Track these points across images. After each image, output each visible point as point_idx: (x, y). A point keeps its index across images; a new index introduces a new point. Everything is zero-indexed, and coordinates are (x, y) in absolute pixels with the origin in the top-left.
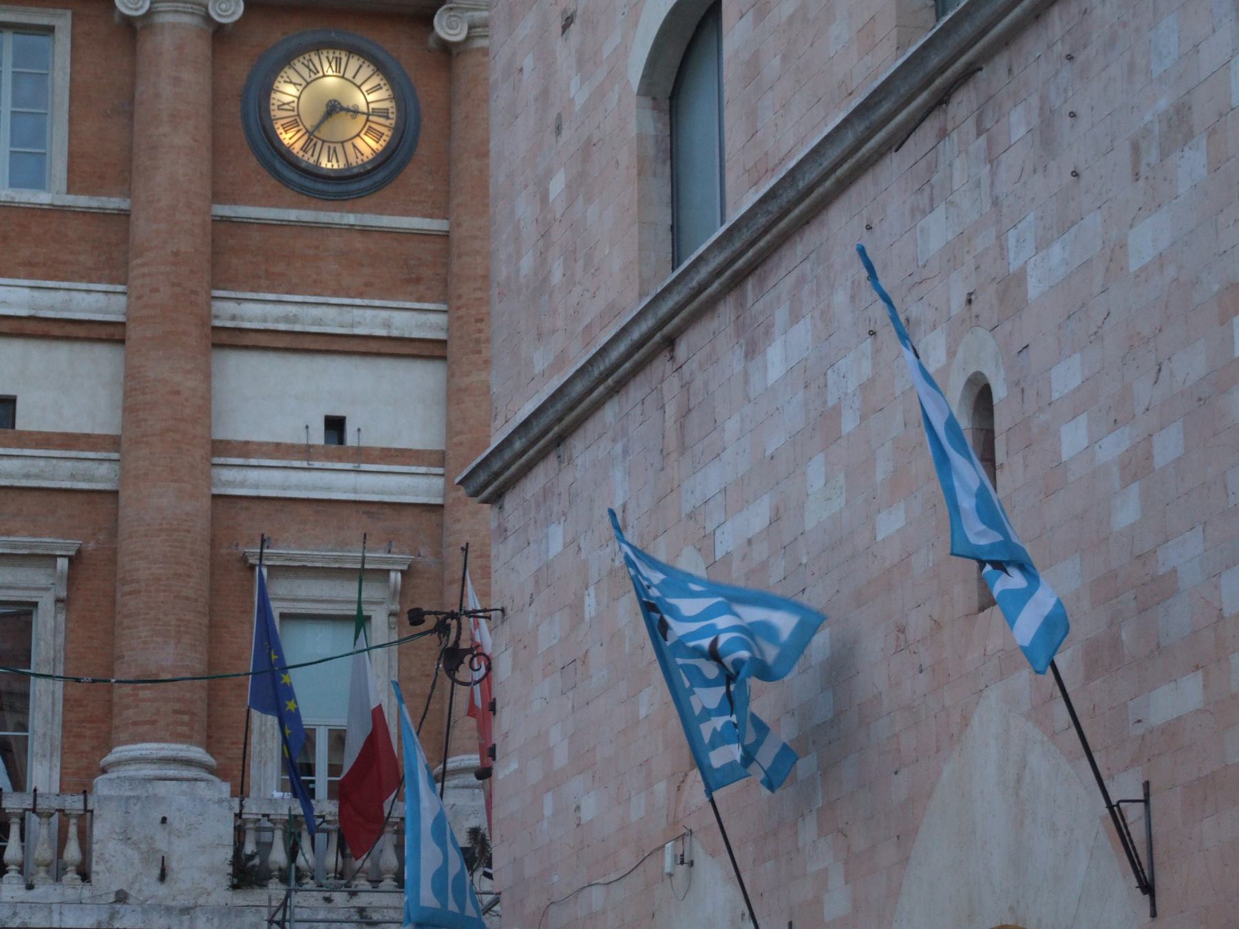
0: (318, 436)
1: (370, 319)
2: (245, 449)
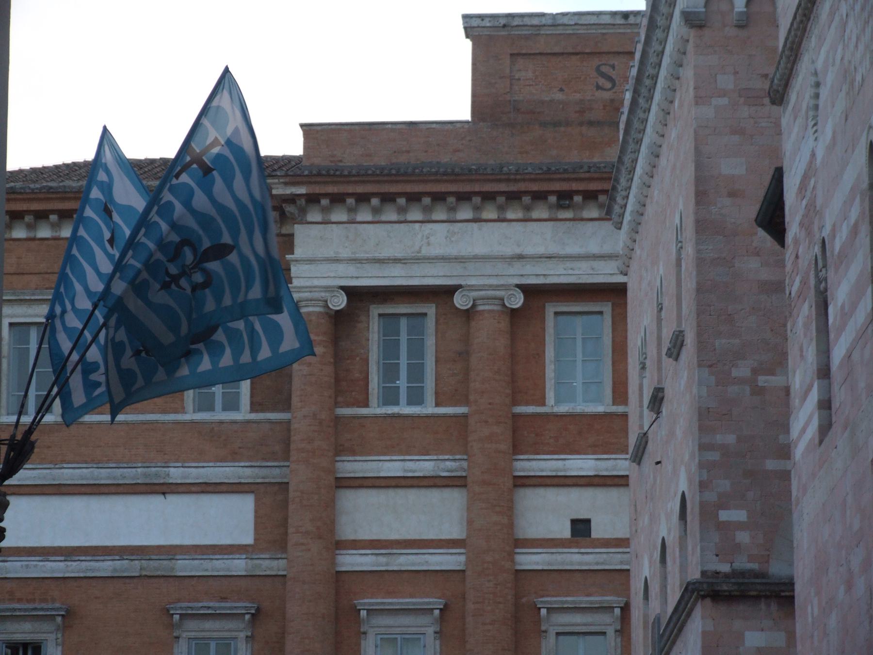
0: (567, 533)
1: (425, 466)
2: (356, 544)
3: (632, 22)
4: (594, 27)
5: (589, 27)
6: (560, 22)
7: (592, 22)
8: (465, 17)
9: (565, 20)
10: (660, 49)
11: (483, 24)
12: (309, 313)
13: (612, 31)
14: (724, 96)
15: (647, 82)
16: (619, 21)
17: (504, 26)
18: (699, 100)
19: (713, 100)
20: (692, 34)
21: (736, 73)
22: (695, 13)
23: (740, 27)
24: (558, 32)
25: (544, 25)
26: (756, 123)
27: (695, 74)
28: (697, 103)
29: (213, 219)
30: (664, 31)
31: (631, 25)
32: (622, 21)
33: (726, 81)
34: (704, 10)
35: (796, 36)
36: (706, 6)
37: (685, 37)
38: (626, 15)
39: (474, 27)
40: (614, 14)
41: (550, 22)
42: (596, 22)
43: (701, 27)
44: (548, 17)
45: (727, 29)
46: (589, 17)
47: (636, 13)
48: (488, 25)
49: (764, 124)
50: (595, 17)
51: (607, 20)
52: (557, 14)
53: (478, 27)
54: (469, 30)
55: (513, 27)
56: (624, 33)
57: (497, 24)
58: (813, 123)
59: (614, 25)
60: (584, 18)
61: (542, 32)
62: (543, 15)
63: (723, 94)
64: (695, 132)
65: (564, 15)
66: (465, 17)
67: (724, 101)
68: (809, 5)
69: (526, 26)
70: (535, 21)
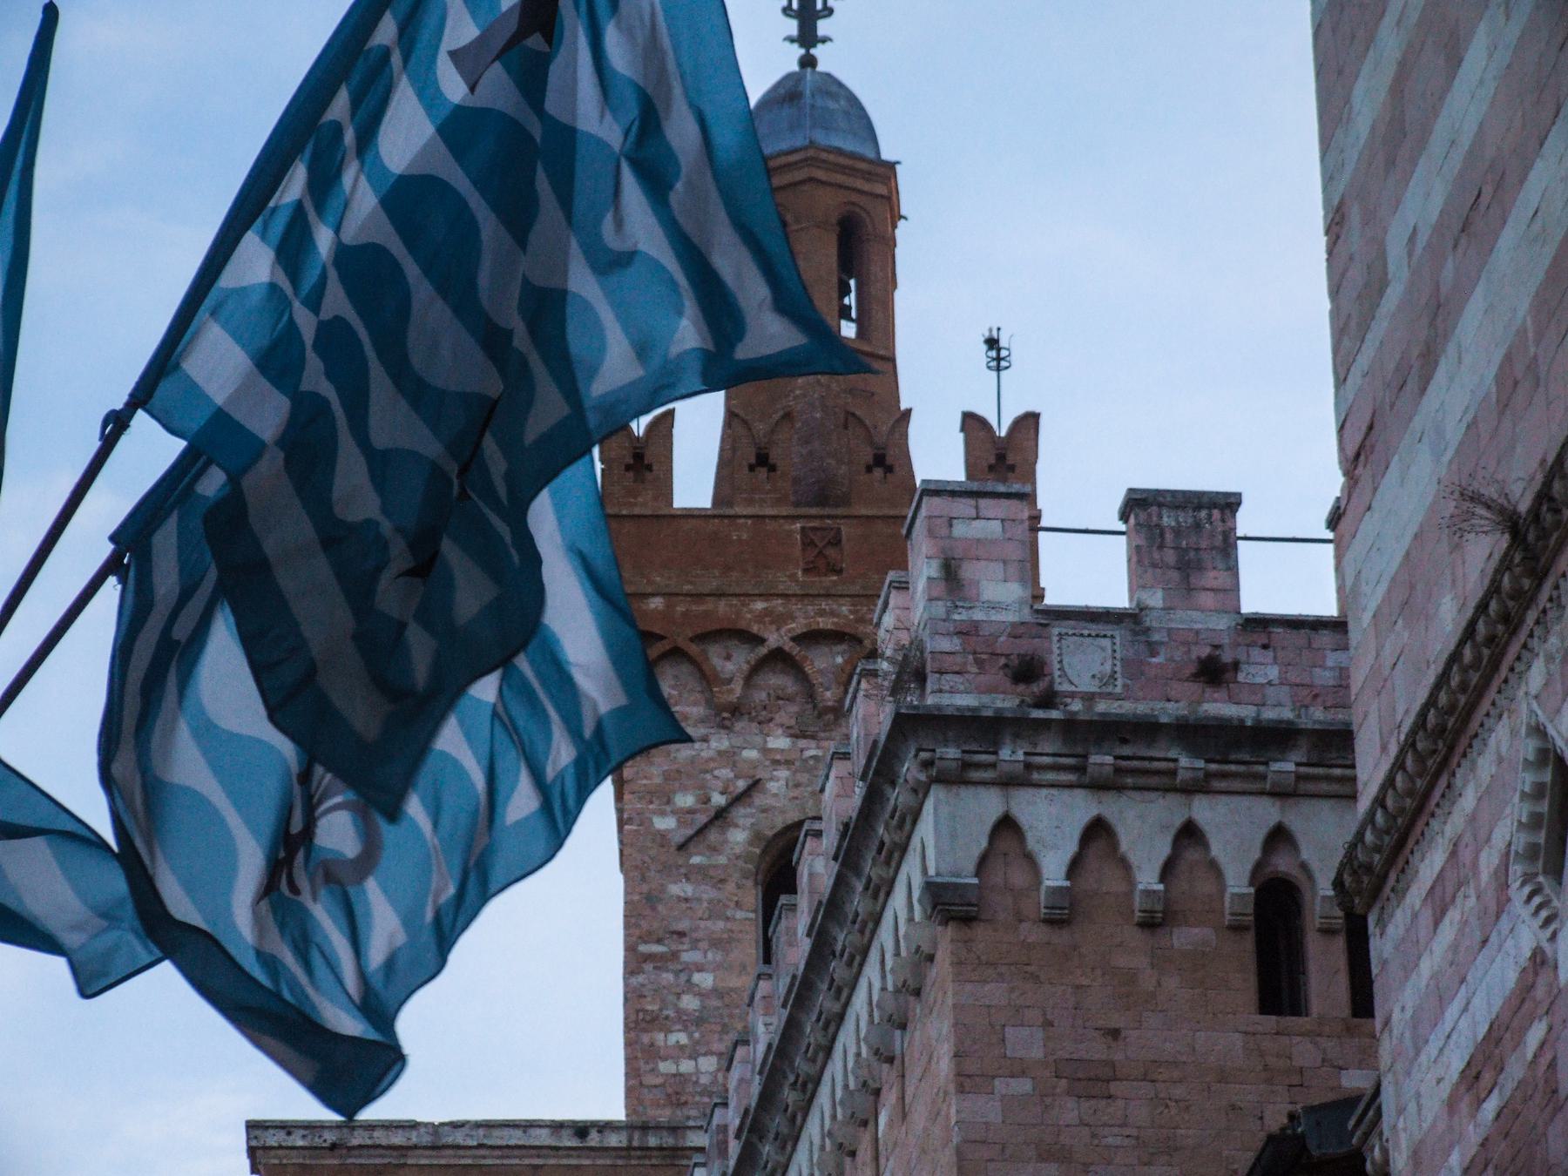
3: (593, 1144)
4: (516, 1152)
5: (506, 1152)
6: (450, 1140)
7: (512, 1142)
8: (252, 1126)
9: (459, 1138)
10: (837, 1007)
11: (290, 1141)
12: (695, 704)
13: (552, 1161)
14: (1023, 1074)
15: (790, 1096)
16: (569, 1141)
17: (333, 1147)
18: (966, 1081)
19: (997, 1082)
20: (945, 940)
21: (1049, 1024)
22: (956, 886)
23: (1050, 922)
24: (443, 1162)
25: (415, 1147)
26: (1094, 1136)
27: (955, 1025)
28: (961, 1090)
29: (326, 402)
30: (850, 964)
31: (592, 1149)
32: (574, 1143)
33: (1027, 1043)
34: (975, 881)
35: (1463, 687)
36: (977, 875)
37: (926, 949)
38: (581, 1129)
39: (272, 1148)
40: (557, 1127)
41: (426, 1140)
42: (520, 1143)
43: (967, 920)
44: (422, 1130)
45: (1025, 926)
46: (506, 1132)
47: (605, 1127)
48: (300, 1143)
49: (1110, 1140)
50: (519, 1133)
51: (543, 1138)
52: (442, 1124)
53: (281, 1147)
54: (259, 1153)
55: (350, 1149)
56: (577, 1167)
57: (317, 1142)
58: (1527, 889)
59: (557, 1148)
60: (496, 1132)
61: (410, 1162)
62: (413, 1125)
63: (1020, 1070)
64: (959, 1152)
65: (456, 1125)
66: (252, 1126)
67: (1023, 1086)
68: (1526, 583)
69: (379, 1146)
70: (398, 1139)
